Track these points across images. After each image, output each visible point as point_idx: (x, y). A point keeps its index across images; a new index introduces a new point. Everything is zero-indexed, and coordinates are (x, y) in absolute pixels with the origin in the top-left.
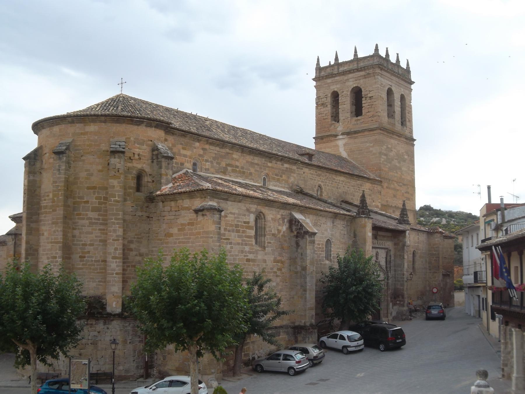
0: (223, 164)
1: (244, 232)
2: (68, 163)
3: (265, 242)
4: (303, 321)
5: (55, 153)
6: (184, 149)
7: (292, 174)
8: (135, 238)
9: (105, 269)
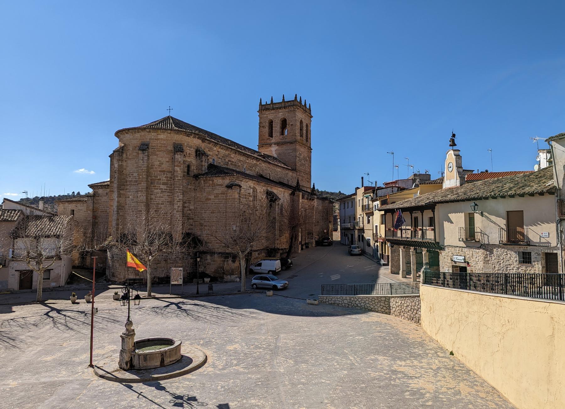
0: (227, 160)
2: (148, 156)
6: (209, 151)
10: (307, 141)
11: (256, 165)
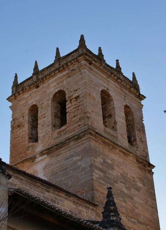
10: (131, 140)
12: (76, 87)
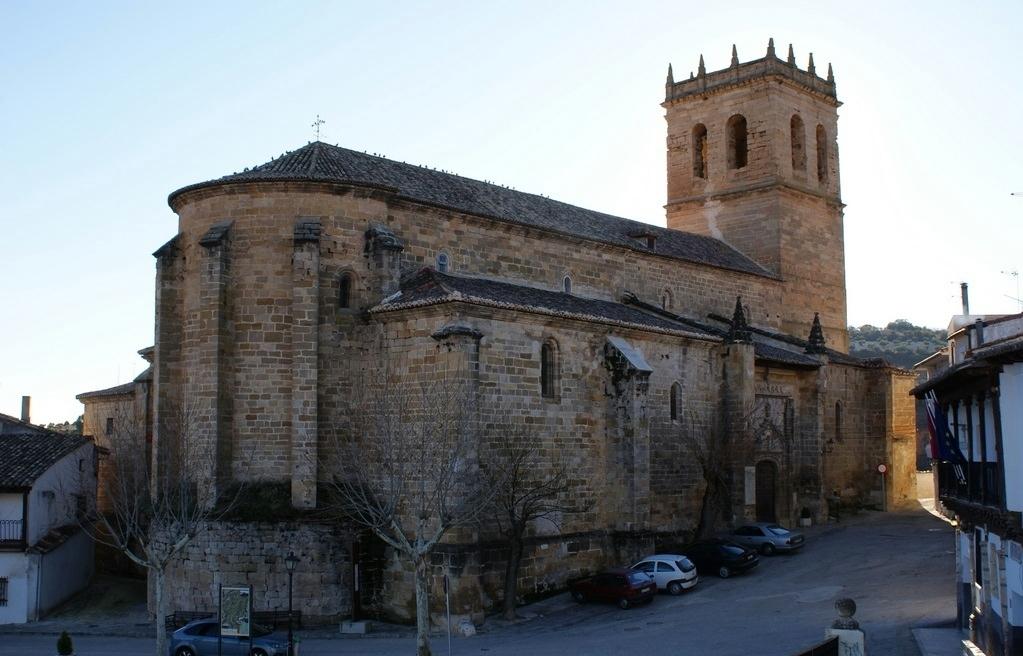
0: (493, 257)
1: (521, 372)
3: (559, 388)
4: (629, 524)
5: (203, 244)
6: (423, 232)
7: (617, 271)
8: (339, 384)
9: (289, 437)
11: (612, 266)
12: (761, 118)
